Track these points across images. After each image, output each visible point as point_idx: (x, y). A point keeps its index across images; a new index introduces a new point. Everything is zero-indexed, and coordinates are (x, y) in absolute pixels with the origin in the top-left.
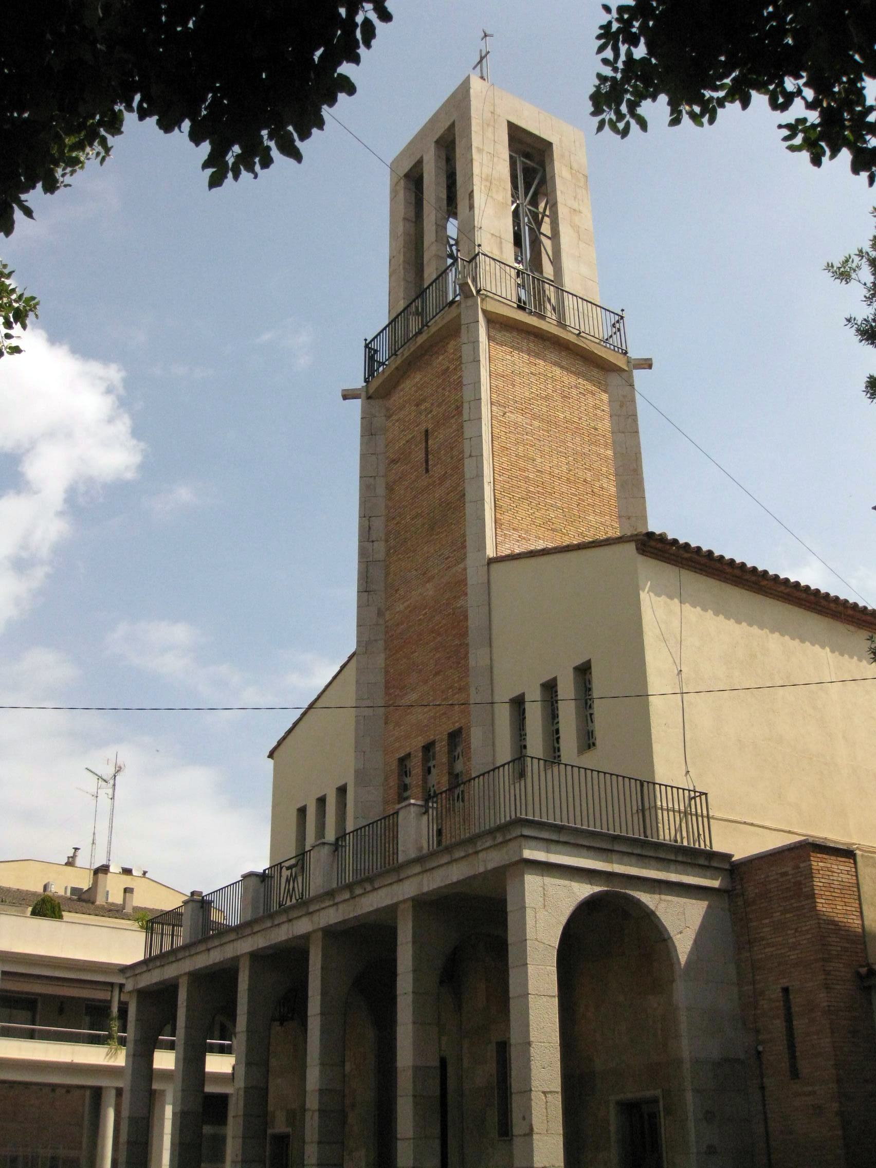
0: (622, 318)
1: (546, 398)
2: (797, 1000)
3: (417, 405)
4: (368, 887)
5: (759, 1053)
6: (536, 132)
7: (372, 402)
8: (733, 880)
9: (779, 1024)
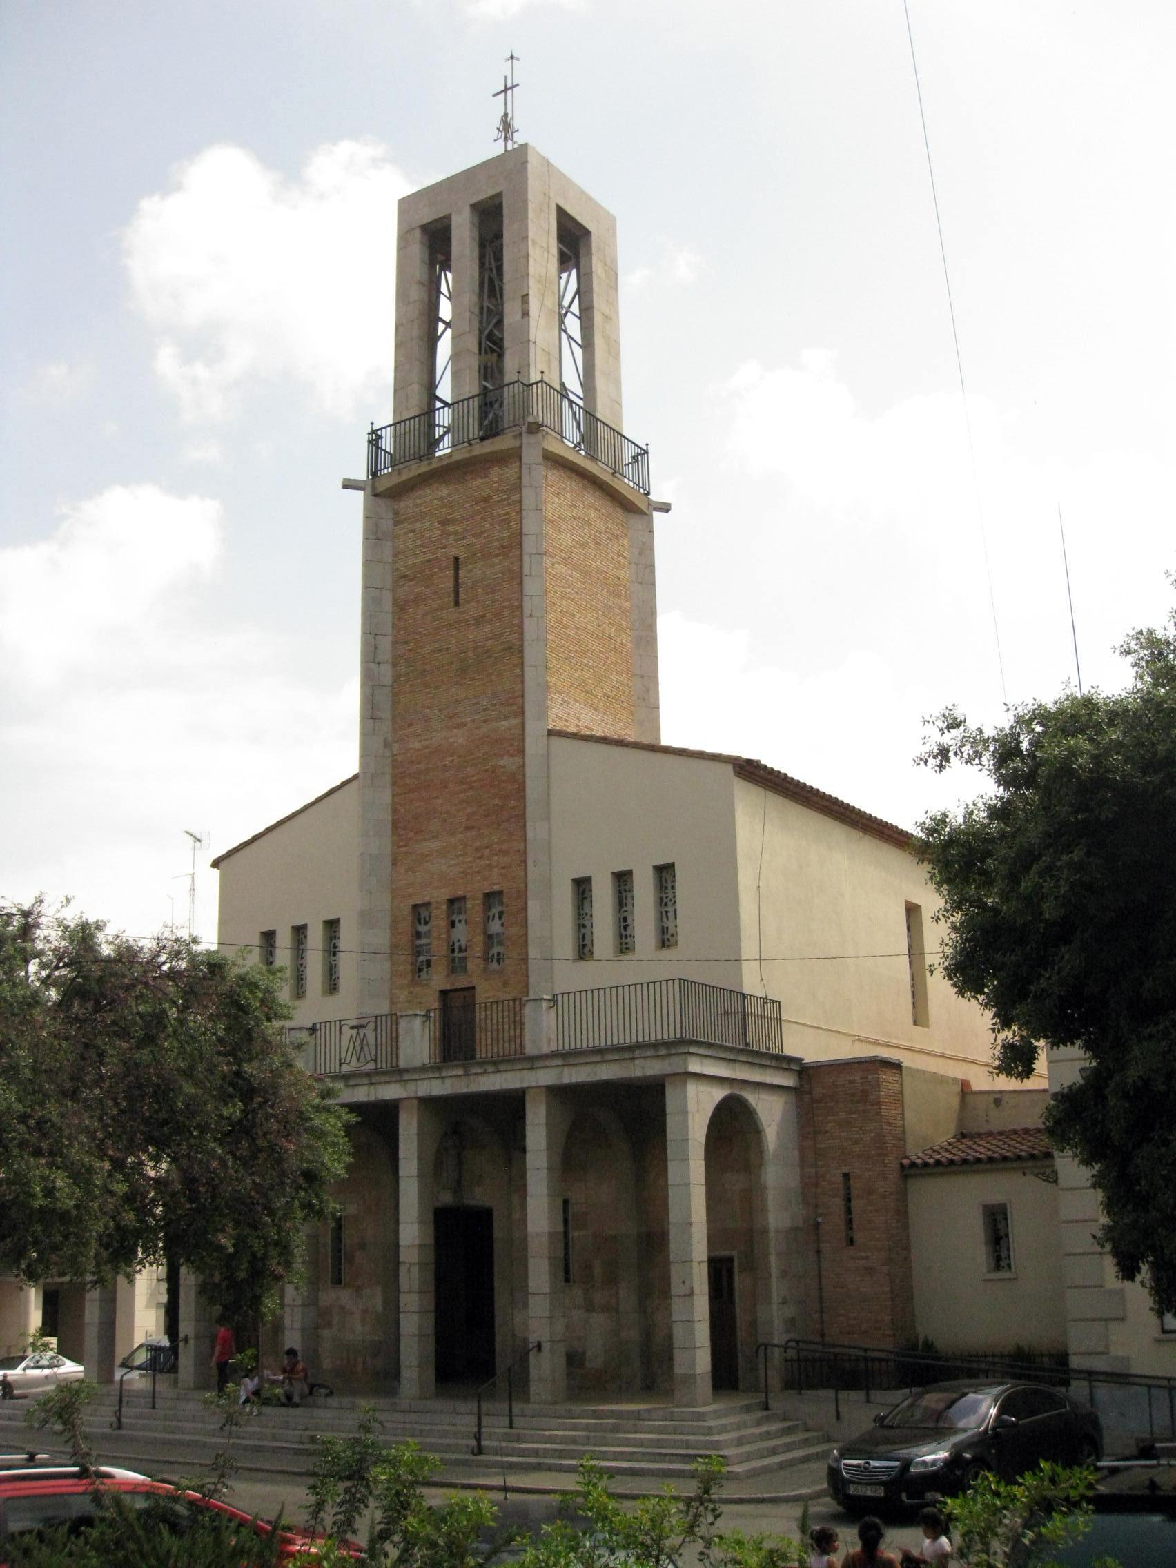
0: (646, 452)
1: (584, 545)
2: (856, 1185)
3: (444, 523)
4: (491, 1069)
5: (818, 1223)
6: (579, 219)
7: (379, 501)
8: (801, 1078)
9: (838, 1203)
